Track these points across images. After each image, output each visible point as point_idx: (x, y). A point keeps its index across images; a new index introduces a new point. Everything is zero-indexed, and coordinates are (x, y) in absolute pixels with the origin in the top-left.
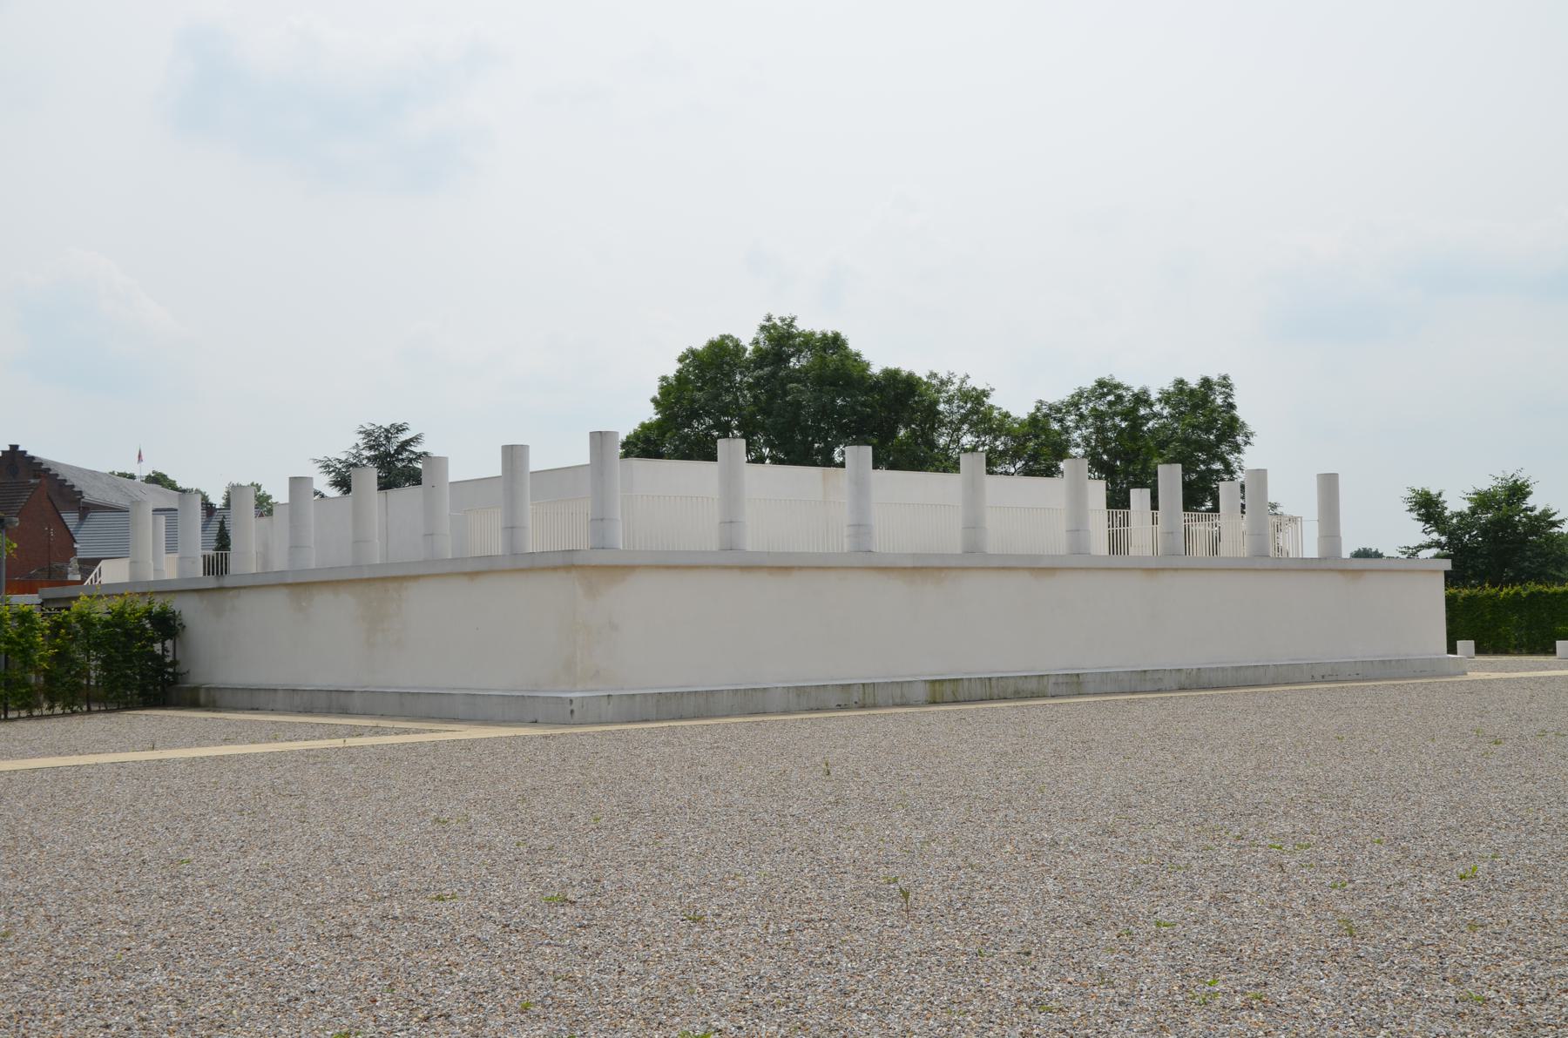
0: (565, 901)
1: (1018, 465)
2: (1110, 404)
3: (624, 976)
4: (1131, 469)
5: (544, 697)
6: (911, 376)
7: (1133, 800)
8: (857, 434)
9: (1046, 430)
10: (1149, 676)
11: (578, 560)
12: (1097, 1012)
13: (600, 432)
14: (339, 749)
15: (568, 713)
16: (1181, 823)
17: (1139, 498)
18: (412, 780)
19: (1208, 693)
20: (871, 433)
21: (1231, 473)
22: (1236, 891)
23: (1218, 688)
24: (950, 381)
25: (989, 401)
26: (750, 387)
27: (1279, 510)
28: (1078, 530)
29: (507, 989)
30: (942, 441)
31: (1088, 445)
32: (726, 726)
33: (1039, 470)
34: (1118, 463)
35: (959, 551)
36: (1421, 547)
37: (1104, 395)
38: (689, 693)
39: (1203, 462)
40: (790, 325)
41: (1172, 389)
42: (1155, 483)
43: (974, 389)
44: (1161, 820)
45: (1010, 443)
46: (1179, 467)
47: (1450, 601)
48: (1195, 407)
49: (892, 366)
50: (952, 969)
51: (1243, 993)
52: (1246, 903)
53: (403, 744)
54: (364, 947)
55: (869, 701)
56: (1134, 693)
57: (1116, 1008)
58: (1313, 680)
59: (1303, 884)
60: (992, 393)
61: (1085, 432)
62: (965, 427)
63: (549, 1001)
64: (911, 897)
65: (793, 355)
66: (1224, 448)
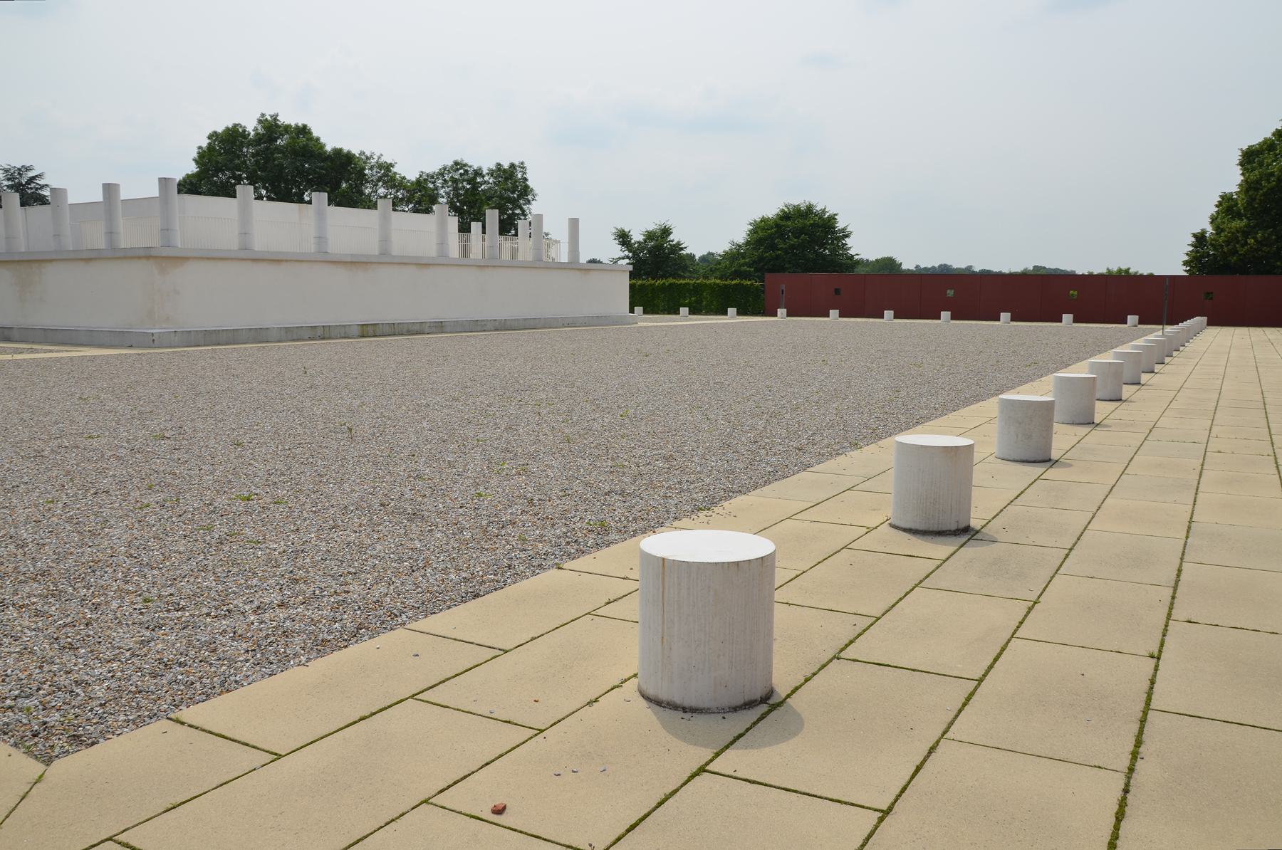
0: (164, 437)
1: (410, 207)
2: (461, 174)
3: (202, 471)
4: (472, 211)
5: (136, 332)
6: (349, 152)
7: (468, 384)
8: (318, 185)
9: (425, 188)
10: (479, 323)
11: (153, 253)
12: (447, 479)
13: (165, 178)
14: (10, 361)
15: (151, 341)
16: (492, 395)
17: (476, 227)
18: (60, 377)
19: (510, 332)
20: (326, 185)
21: (525, 215)
22: (517, 425)
23: (515, 330)
24: (371, 157)
25: (394, 170)
26: (253, 155)
27: (549, 237)
28: (442, 244)
29: (139, 479)
30: (367, 191)
31: (449, 197)
32: (245, 349)
33: (421, 210)
34: (465, 207)
35: (377, 253)
36: (620, 258)
37: (458, 170)
38: (223, 330)
39: (511, 209)
40: (275, 119)
41: (494, 168)
42: (485, 218)
43: (385, 162)
44: (482, 393)
45: (406, 194)
46: (497, 211)
47: (632, 287)
48: (506, 179)
49: (338, 146)
50: (375, 463)
51: (516, 468)
52: (521, 430)
53: (51, 358)
54: (50, 462)
55: (327, 335)
56: (471, 332)
57: (456, 477)
58: (564, 326)
59: (549, 421)
60: (396, 165)
61: (447, 190)
62: (380, 184)
63: (163, 484)
64: (353, 432)
65: (278, 138)
66: (521, 202)
